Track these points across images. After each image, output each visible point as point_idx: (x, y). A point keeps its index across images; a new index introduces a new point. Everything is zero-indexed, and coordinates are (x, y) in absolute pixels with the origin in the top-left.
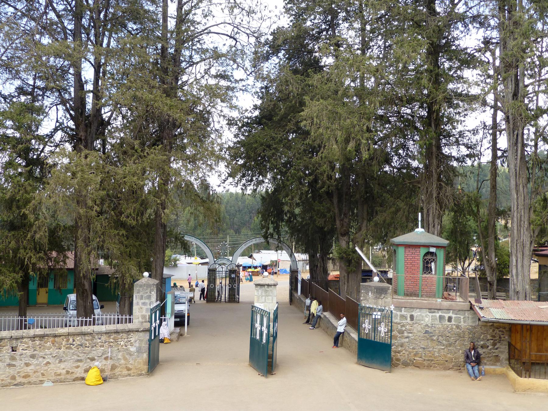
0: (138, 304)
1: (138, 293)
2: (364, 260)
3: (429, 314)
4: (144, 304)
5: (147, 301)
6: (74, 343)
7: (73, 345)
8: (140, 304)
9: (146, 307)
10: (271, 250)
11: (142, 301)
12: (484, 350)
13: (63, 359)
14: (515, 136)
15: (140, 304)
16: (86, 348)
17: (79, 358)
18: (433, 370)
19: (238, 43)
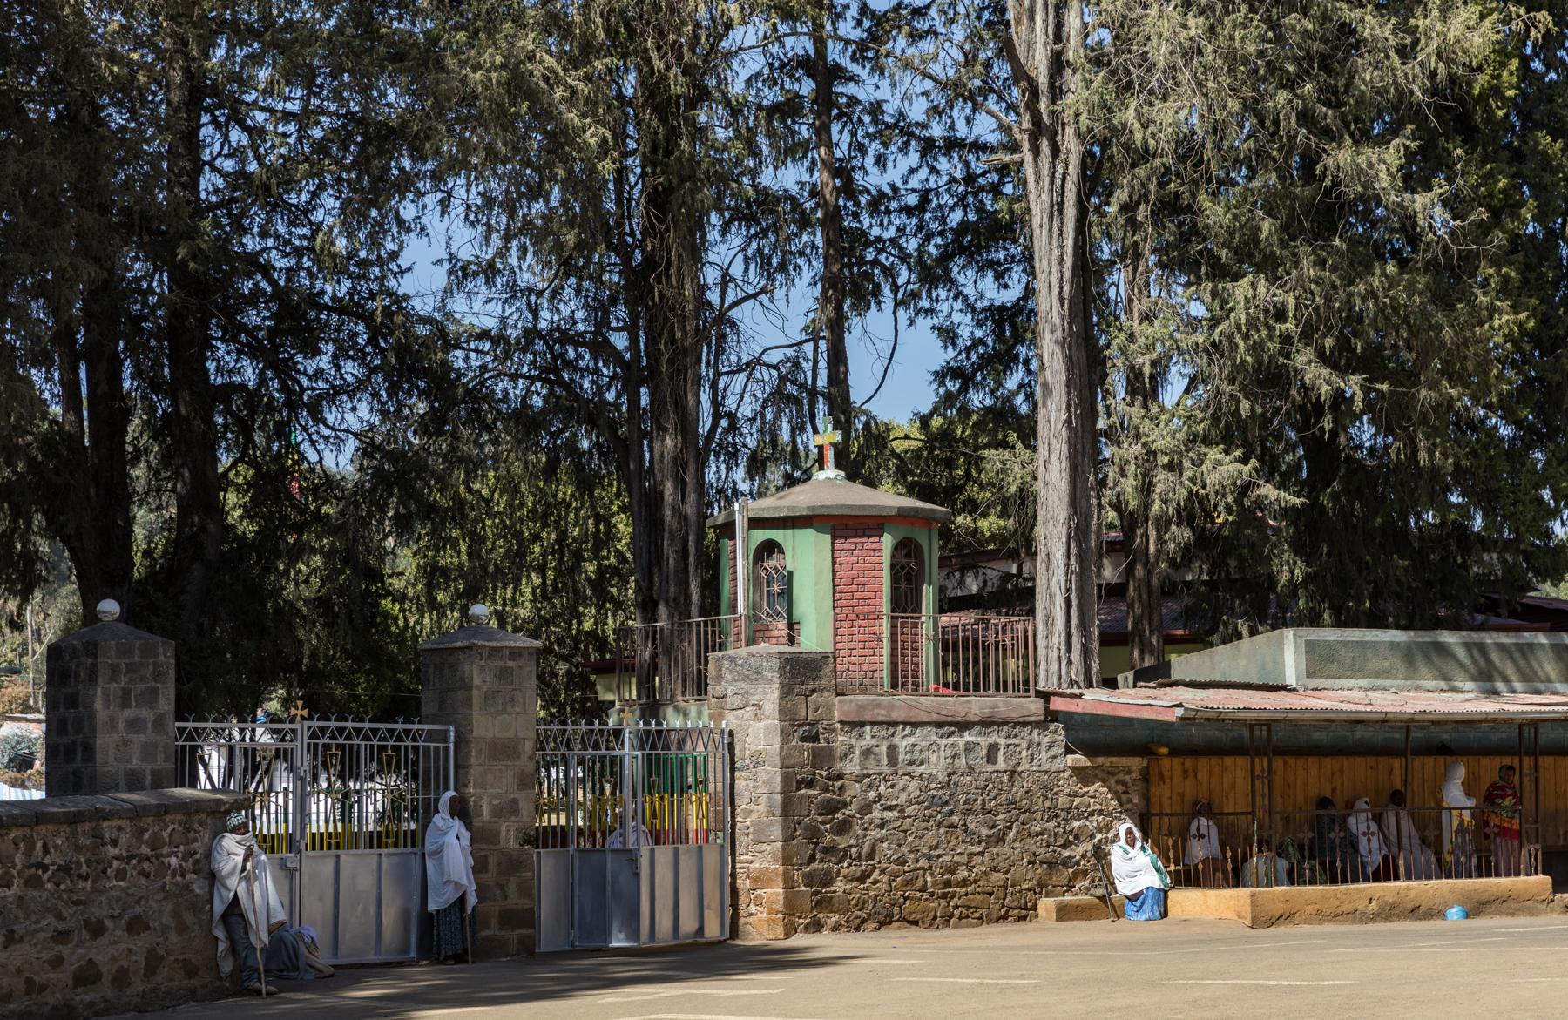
0: (112, 724)
1: (112, 680)
2: (1079, 532)
3: (939, 741)
4: (134, 725)
5: (147, 714)
6: (47, 861)
7: (45, 868)
8: (121, 726)
9: (142, 738)
10: (1387, 627)
11: (127, 713)
12: (1001, 758)
13: (20, 929)
14: (1058, 182)
15: (121, 726)
16: (81, 884)
17: (61, 926)
18: (956, 926)
19: (766, 358)
